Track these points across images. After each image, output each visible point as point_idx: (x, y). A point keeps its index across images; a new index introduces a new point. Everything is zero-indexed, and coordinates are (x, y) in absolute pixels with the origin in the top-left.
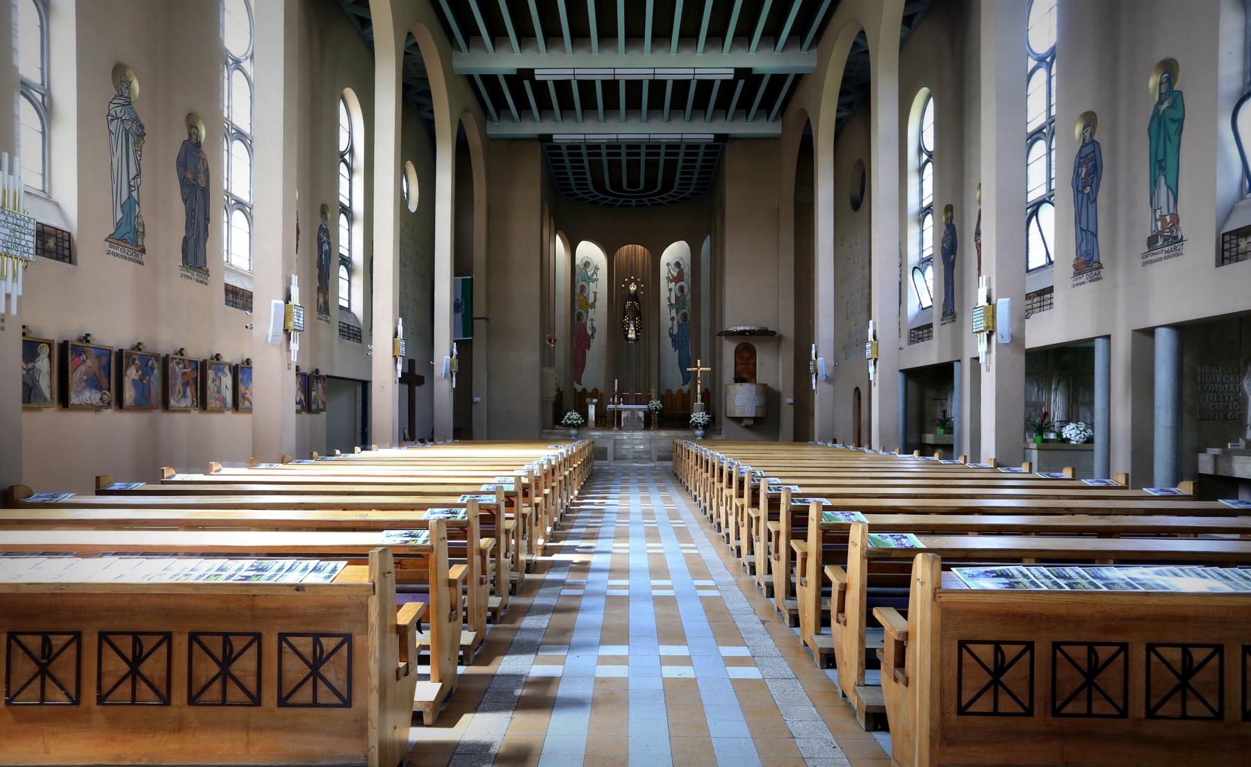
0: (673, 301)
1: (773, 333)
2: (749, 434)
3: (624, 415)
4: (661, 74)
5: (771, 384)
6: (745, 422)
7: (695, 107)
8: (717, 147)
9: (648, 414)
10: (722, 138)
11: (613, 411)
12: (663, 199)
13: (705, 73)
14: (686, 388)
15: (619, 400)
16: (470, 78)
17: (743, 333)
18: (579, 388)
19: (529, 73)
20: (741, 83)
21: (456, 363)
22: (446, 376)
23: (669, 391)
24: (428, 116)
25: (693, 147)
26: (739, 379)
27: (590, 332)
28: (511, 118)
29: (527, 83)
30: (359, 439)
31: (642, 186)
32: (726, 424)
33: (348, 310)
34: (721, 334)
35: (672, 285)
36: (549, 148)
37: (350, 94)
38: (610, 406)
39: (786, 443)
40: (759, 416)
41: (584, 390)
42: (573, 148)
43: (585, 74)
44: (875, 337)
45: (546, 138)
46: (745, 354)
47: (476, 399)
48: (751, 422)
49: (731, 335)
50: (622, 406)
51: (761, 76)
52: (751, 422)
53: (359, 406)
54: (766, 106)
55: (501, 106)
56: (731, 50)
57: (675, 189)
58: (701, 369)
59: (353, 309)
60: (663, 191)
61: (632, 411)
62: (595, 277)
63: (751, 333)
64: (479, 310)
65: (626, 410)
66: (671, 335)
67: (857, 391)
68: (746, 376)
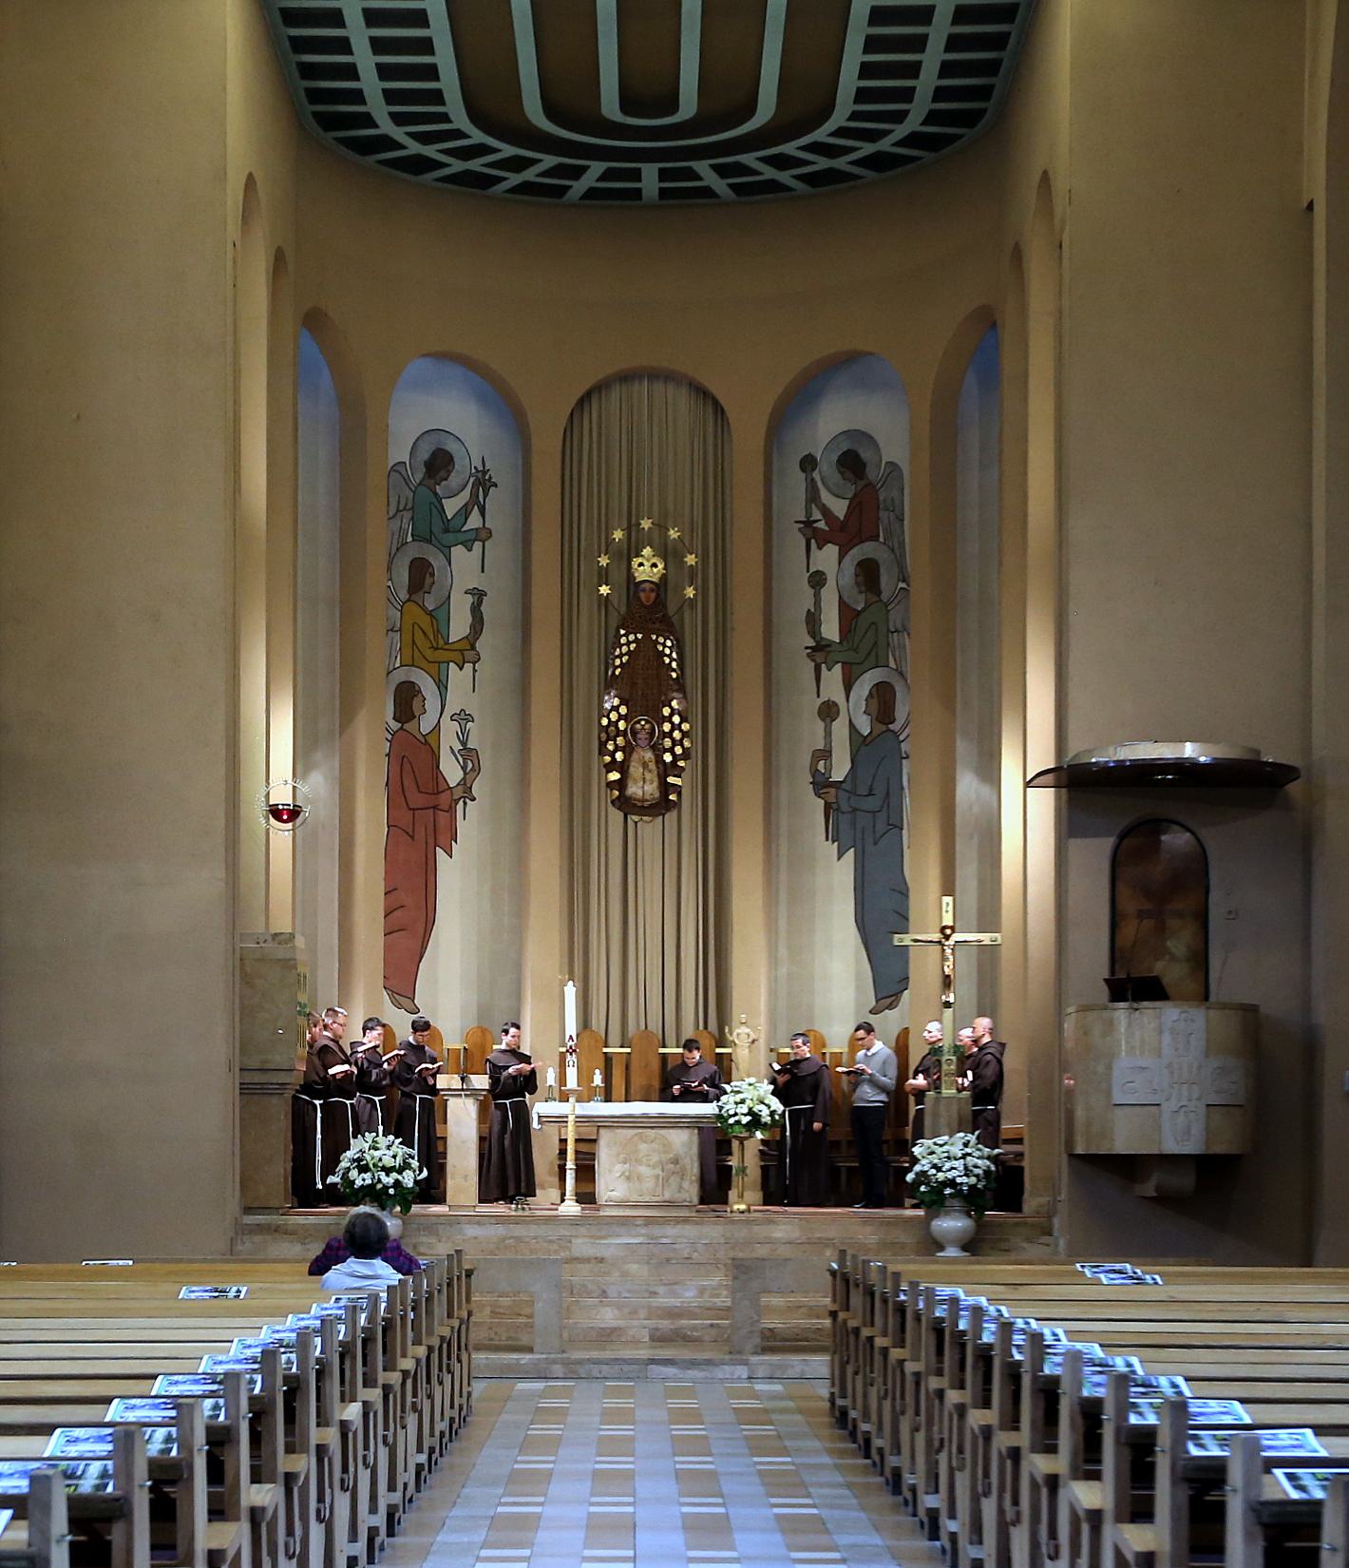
0: (831, 630)
12: (781, 162)
15: (584, 1077)
27: (452, 772)
31: (688, 105)
35: (827, 557)
52: (1185, 1181)
57: (839, 118)
62: (474, 521)
66: (821, 784)
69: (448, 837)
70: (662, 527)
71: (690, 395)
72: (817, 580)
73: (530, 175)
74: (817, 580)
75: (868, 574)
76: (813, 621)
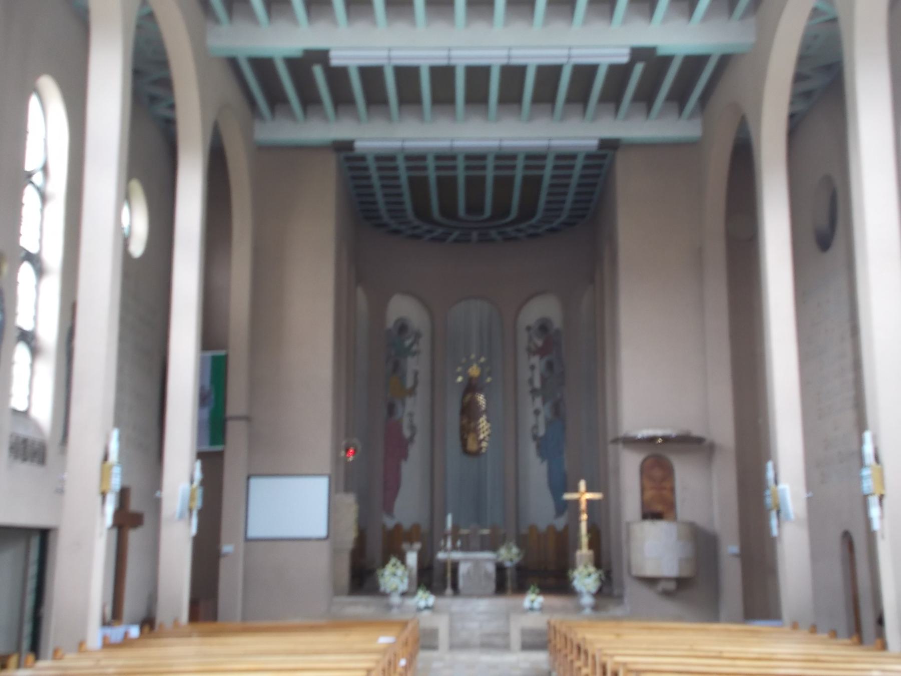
0: (537, 384)
1: (699, 441)
2: (670, 606)
3: (463, 569)
4: (519, 57)
5: (701, 520)
6: (662, 586)
7: (569, 100)
8: (603, 157)
9: (500, 569)
10: (609, 146)
11: (444, 564)
12: (519, 231)
13: (584, 55)
14: (560, 523)
15: (454, 543)
16: (233, 63)
17: (652, 440)
18: (390, 523)
19: (322, 56)
20: (639, 68)
21: (199, 493)
22: (181, 517)
23: (533, 528)
24: (167, 113)
25: (565, 158)
26: (650, 514)
27: (407, 433)
28: (291, 114)
29: (318, 71)
30: (26, 643)
31: (488, 212)
32: (632, 590)
33: (25, 414)
34: (616, 441)
35: (535, 360)
36: (348, 159)
37: (48, 85)
38: (441, 555)
39: (732, 620)
40: (686, 573)
41: (398, 527)
42: (386, 160)
43: (406, 56)
44: (877, 458)
45: (344, 147)
46: (657, 473)
47: (227, 548)
48: (672, 586)
49: (632, 442)
50: (456, 555)
51: (667, 60)
52: (672, 586)
53: (33, 570)
54: (679, 97)
55: (276, 99)
56: (625, 21)
57: (539, 215)
58: (584, 496)
59: (35, 413)
60: (521, 218)
61: (477, 562)
62: (415, 348)
63: (666, 439)
64: (236, 404)
65: (466, 560)
66: (535, 437)
67: (848, 540)
68: (659, 508)
69: (405, 456)
70: (478, 358)
71: (130, 227)
72: (532, 368)
73: (435, 234)
74: (532, 368)
75: (550, 366)
76: (531, 381)
